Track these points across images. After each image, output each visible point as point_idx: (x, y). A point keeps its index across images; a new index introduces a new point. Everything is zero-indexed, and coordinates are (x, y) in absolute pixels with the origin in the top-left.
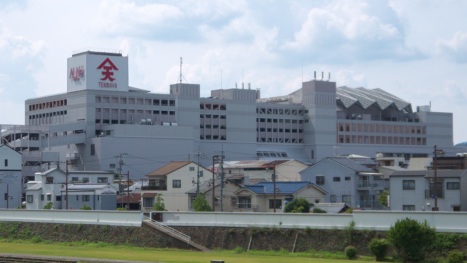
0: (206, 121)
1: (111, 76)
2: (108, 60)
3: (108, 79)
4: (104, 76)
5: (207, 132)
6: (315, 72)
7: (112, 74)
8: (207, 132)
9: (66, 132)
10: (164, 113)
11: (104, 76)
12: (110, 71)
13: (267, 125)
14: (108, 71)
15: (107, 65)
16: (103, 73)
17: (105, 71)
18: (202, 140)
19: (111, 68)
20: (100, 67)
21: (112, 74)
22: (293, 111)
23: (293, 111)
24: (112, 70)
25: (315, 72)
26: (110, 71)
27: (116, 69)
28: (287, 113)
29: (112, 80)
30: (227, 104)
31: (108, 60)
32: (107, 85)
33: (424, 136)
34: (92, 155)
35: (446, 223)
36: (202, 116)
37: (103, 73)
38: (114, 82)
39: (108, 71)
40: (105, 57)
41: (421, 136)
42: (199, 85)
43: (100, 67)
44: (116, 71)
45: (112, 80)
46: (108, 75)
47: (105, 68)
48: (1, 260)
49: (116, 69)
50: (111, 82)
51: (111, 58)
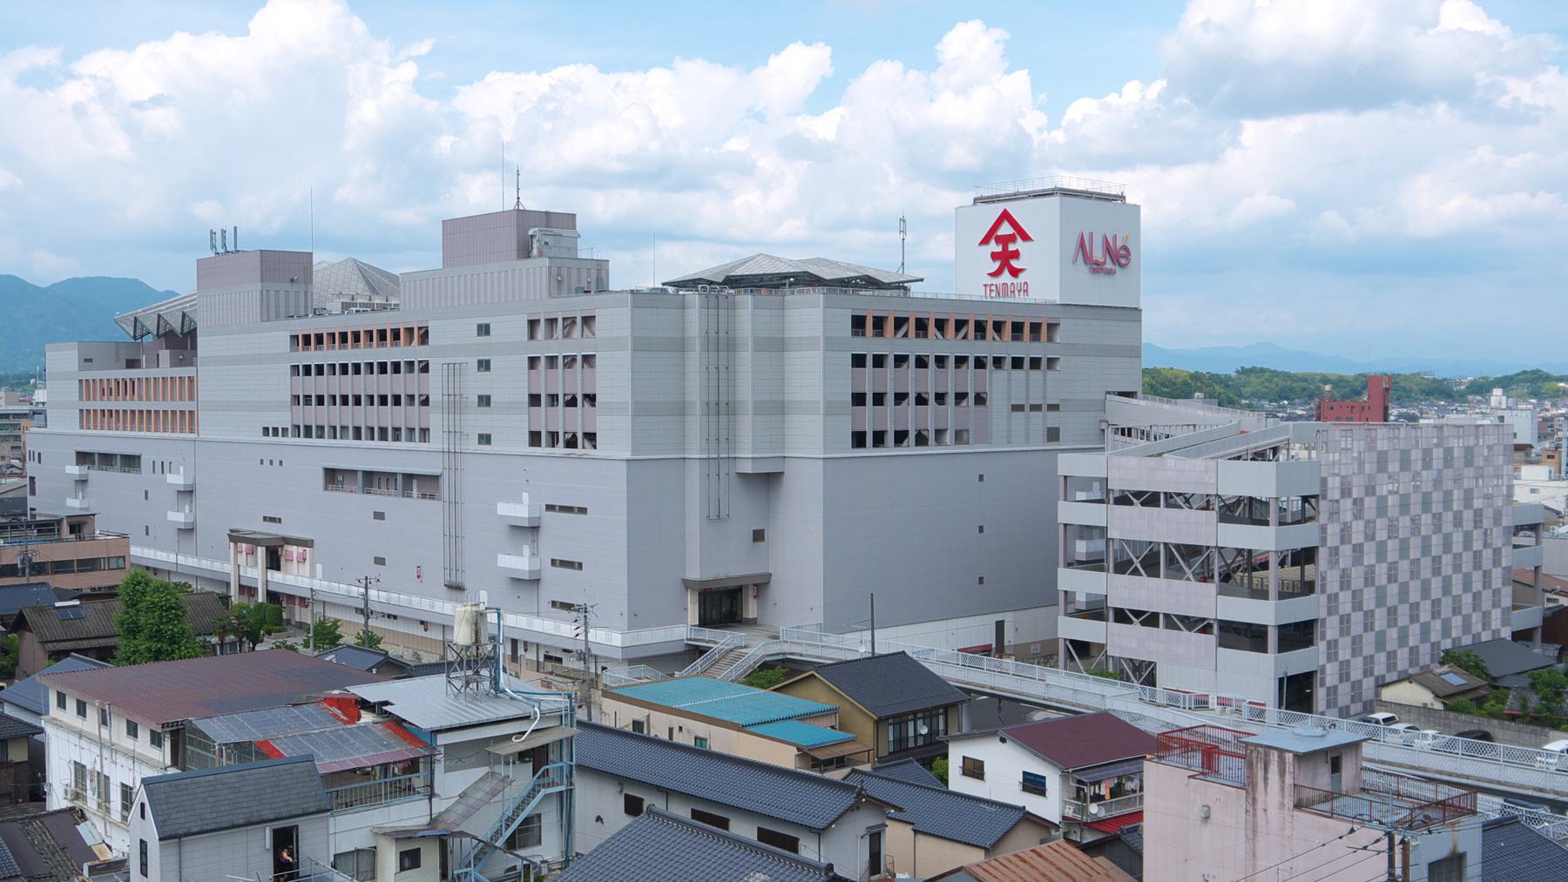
0: (869, 380)
1: (1014, 263)
2: (1005, 216)
3: (1006, 275)
5: (869, 419)
6: (583, 511)
7: (1016, 254)
8: (869, 419)
9: (1518, 448)
10: (1017, 363)
11: (997, 264)
12: (1012, 247)
13: (889, 380)
14: (1005, 248)
15: (1006, 229)
16: (994, 256)
17: (999, 249)
19: (1012, 238)
20: (985, 241)
21: (1016, 254)
22: (957, 322)
23: (957, 322)
24: (1019, 245)
25: (583, 511)
27: (1026, 237)
28: (961, 334)
29: (1015, 272)
31: (1005, 216)
33: (191, 406)
34: (78, 454)
36: (858, 361)
37: (994, 256)
38: (1022, 277)
39: (1005, 248)
40: (995, 210)
42: (574, 216)
43: (985, 241)
44: (1028, 243)
45: (1015, 272)
46: (1006, 259)
47: (999, 240)
49: (1026, 237)
50: (1015, 281)
51: (1014, 209)
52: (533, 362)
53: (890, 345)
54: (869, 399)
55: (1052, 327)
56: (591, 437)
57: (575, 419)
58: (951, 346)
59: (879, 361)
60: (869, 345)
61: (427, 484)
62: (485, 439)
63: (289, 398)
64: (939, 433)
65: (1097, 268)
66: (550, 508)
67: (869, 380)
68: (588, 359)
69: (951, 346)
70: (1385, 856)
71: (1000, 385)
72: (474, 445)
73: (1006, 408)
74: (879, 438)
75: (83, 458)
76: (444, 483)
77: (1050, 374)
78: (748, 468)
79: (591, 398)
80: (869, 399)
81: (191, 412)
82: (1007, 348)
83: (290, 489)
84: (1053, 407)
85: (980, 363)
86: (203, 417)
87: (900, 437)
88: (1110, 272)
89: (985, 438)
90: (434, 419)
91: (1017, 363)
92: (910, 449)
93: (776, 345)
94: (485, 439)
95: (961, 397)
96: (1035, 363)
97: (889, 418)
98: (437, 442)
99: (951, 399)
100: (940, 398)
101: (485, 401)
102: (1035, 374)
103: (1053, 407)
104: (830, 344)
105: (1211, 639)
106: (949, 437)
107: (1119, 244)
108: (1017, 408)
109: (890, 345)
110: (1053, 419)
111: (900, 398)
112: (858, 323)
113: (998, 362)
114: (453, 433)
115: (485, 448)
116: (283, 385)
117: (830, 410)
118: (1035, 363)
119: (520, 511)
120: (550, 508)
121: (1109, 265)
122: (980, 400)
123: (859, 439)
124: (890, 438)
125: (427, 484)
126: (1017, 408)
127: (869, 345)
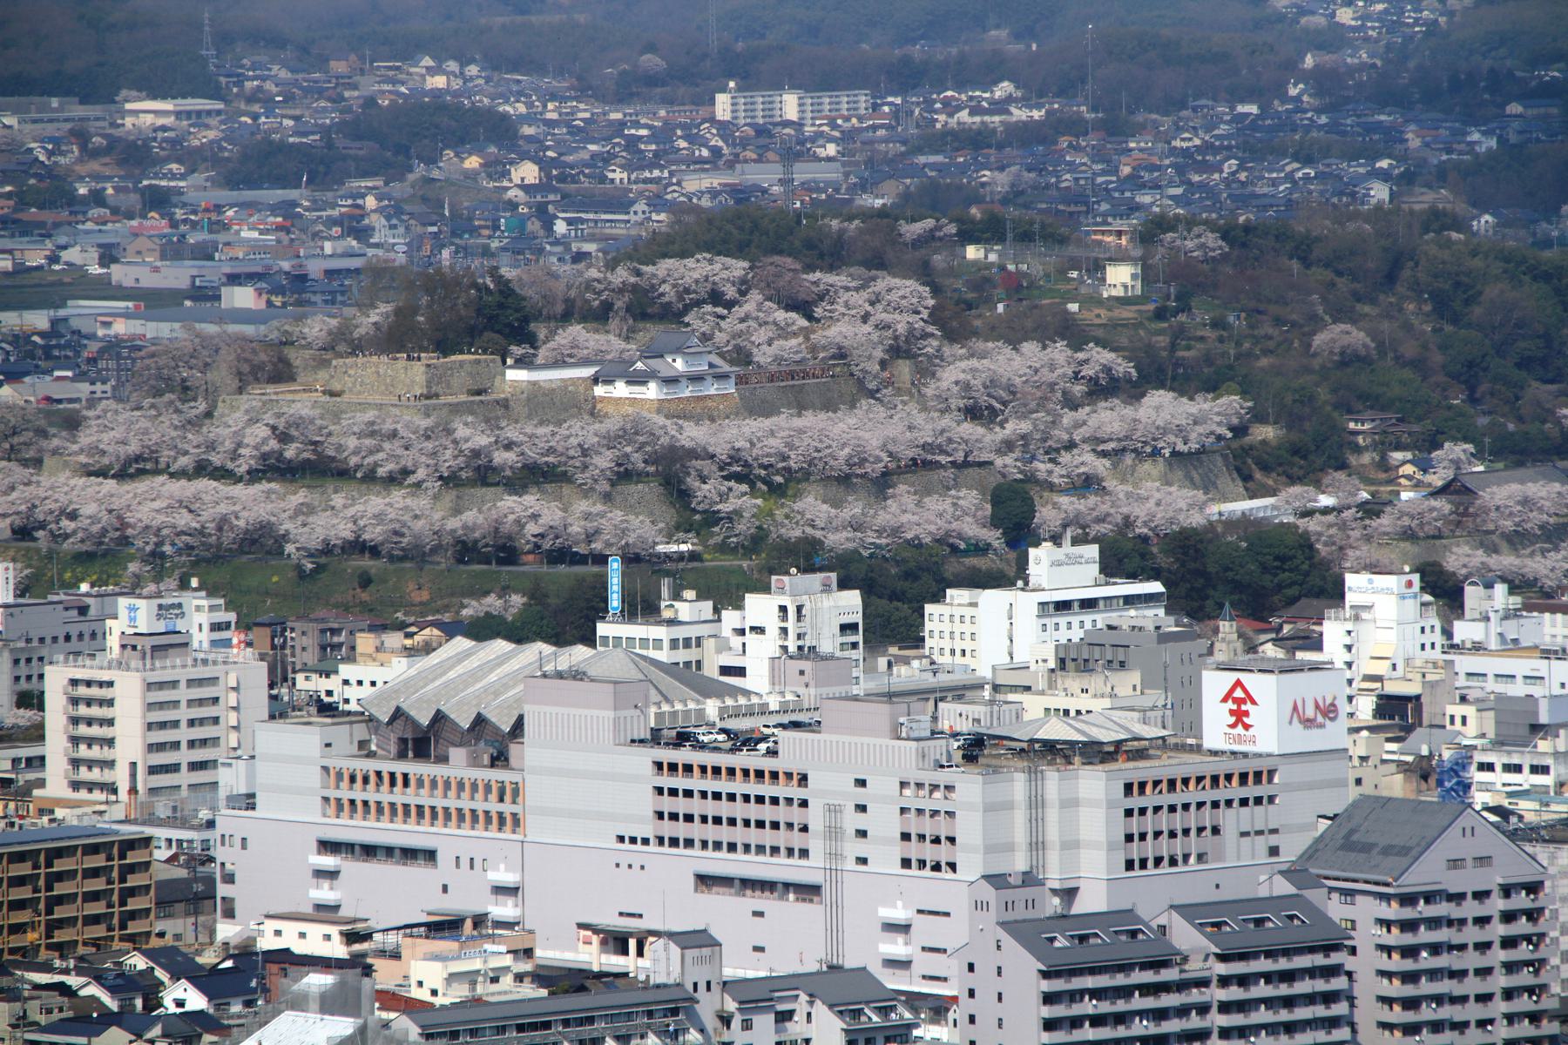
0: (1135, 825)
2: (1238, 683)
4: (1232, 720)
6: (947, 914)
7: (1247, 713)
10: (1244, 802)
11: (1232, 720)
12: (1244, 708)
15: (1239, 693)
16: (1232, 712)
18: (621, 846)
20: (1225, 700)
21: (1247, 713)
25: (947, 914)
26: (1244, 708)
27: (1254, 702)
29: (1247, 727)
30: (1082, 884)
31: (1238, 683)
32: (1239, 739)
35: (4, 463)
37: (1232, 712)
38: (1251, 732)
41: (507, 808)
43: (1225, 700)
45: (1247, 727)
48: (1558, 533)
49: (1254, 702)
52: (903, 810)
53: (1150, 799)
54: (1136, 837)
55: (1271, 773)
56: (952, 866)
57: (943, 853)
58: (1192, 795)
59: (1143, 811)
60: (1136, 802)
61: (808, 891)
62: (863, 861)
63: (651, 814)
64: (1186, 857)
65: (1308, 723)
66: (920, 912)
67: (1135, 825)
68: (950, 814)
69: (1192, 795)
70: (1053, 780)
71: (1232, 820)
72: (850, 864)
73: (1235, 834)
74: (1143, 864)
75: (327, 846)
76: (826, 891)
77: (1271, 807)
78: (1057, 885)
79: (952, 840)
80: (1136, 837)
81: (514, 815)
82: (1235, 791)
83: (664, 891)
84: (1274, 831)
85: (1215, 805)
86: (530, 821)
87: (1158, 861)
88: (1322, 726)
89: (1221, 858)
90: (815, 844)
91: (1244, 802)
92: (1165, 868)
93: (1070, 803)
94: (863, 861)
95: (1200, 830)
96: (1258, 801)
97: (1149, 849)
98: (817, 859)
99: (1193, 833)
100: (1172, 835)
101: (862, 834)
102: (1259, 809)
103: (1274, 831)
104: (1111, 805)
105: (1398, 1034)
106: (1192, 860)
107: (1328, 701)
108: (1244, 834)
109: (1150, 799)
110: (1273, 840)
111: (1172, 835)
112: (1128, 788)
113: (1229, 803)
114: (834, 855)
115: (862, 868)
116: (649, 803)
117: (1111, 847)
118: (1258, 801)
119: (899, 914)
120: (920, 912)
121: (1320, 719)
122: (1216, 831)
123: (1129, 865)
124: (1150, 863)
125: (808, 891)
126: (1244, 834)
127: (1136, 802)
